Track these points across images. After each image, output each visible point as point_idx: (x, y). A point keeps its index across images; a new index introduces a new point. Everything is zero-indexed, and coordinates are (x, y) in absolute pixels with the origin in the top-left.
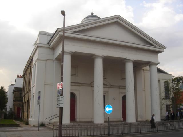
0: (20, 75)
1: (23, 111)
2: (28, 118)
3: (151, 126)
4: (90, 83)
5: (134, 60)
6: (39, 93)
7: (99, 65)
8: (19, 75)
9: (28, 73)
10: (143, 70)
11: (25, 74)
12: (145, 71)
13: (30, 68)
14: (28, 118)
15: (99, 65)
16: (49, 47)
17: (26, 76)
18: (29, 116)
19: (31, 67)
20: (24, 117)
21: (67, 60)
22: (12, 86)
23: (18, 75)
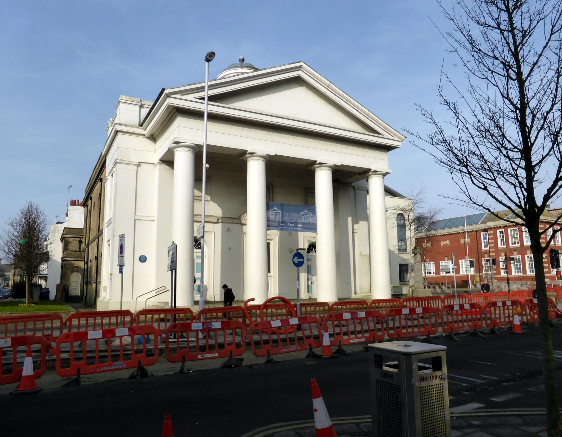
0: (78, 201)
1: (85, 280)
2: (95, 298)
3: (535, 283)
4: (237, 217)
5: (335, 165)
6: (122, 237)
7: (256, 174)
8: (75, 201)
9: (95, 195)
10: (354, 187)
11: (88, 197)
12: (356, 191)
13: (99, 182)
14: (95, 298)
15: (256, 174)
16: (144, 135)
17: (91, 203)
18: (99, 289)
19: (101, 180)
20: (87, 295)
21: (183, 159)
22: (59, 225)
23: (74, 200)
